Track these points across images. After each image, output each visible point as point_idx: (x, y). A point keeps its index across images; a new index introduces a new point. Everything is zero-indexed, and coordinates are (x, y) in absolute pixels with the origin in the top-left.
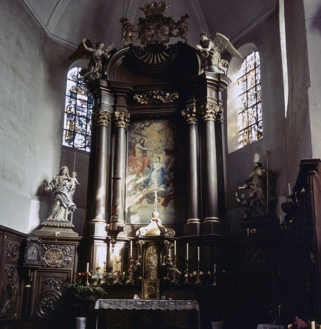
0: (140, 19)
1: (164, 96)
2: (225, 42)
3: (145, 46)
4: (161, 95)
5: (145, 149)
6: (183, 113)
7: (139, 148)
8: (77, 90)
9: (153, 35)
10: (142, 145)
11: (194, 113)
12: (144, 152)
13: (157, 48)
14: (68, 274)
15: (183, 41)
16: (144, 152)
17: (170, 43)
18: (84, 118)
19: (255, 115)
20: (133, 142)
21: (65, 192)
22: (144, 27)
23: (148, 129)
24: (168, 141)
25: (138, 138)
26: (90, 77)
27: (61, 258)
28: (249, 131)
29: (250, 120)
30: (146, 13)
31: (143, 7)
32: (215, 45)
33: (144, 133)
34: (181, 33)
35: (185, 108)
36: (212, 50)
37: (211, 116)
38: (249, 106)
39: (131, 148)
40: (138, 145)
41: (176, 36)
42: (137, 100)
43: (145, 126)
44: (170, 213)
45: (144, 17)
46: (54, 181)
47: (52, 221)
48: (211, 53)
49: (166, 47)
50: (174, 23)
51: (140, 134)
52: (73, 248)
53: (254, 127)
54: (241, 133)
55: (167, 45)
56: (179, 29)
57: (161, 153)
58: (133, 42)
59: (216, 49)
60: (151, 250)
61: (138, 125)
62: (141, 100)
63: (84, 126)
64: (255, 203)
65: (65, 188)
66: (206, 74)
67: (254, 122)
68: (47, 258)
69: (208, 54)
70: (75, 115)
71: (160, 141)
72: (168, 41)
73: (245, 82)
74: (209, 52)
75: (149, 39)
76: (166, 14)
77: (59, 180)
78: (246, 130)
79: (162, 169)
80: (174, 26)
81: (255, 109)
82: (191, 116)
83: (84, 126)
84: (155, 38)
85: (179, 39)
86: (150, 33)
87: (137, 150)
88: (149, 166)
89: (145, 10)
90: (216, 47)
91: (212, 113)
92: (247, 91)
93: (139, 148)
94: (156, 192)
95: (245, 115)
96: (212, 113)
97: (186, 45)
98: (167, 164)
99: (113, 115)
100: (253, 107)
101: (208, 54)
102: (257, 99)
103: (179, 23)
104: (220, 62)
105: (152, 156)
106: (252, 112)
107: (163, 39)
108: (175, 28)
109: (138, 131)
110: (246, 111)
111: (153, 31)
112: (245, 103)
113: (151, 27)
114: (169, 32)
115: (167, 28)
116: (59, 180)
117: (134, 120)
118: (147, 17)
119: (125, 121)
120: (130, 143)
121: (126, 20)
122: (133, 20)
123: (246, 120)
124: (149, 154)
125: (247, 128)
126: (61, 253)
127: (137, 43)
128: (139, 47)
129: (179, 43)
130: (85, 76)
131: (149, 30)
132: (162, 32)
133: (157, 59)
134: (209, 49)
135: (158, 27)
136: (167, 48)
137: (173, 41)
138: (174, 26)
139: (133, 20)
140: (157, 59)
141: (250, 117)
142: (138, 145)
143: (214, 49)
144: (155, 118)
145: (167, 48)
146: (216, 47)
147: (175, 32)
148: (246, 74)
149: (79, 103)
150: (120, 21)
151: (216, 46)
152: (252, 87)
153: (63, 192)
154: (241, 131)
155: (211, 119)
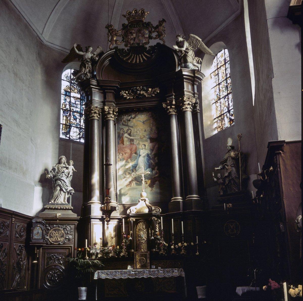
0: (123, 25)
1: (147, 91)
2: (197, 41)
3: (129, 48)
4: (144, 90)
5: (132, 138)
6: (164, 105)
7: (127, 138)
8: (71, 89)
9: (135, 38)
10: (130, 134)
11: (173, 105)
12: (132, 141)
13: (138, 49)
14: (69, 250)
15: (162, 42)
16: (132, 141)
17: (150, 44)
18: (78, 113)
19: (227, 104)
20: (121, 132)
21: (64, 178)
22: (126, 32)
23: (134, 120)
24: (151, 130)
25: (126, 129)
26: (82, 77)
27: (62, 236)
28: (222, 119)
29: (222, 109)
30: (128, 19)
31: (125, 14)
32: (189, 45)
33: (131, 124)
34: (159, 35)
35: (165, 101)
36: (187, 49)
37: (188, 107)
38: (221, 97)
39: (120, 138)
40: (126, 135)
41: (155, 38)
42: (123, 96)
43: (131, 118)
44: (156, 193)
45: (126, 22)
46: (54, 169)
47: (54, 204)
48: (186, 52)
49: (147, 48)
50: (153, 27)
51: (127, 125)
52: (73, 227)
53: (226, 115)
54: (215, 121)
55: (147, 46)
56: (157, 31)
57: (146, 141)
58: (118, 45)
59: (190, 48)
60: (141, 226)
61: (125, 118)
62: (127, 95)
63: (78, 120)
64: (230, 181)
65: (64, 175)
66: (182, 70)
67: (226, 111)
68: (51, 237)
69: (183, 53)
70: (70, 111)
71: (145, 131)
72: (149, 43)
73: (217, 76)
74: (184, 51)
75: (132, 42)
76: (146, 19)
77: (58, 168)
78: (220, 118)
79: (148, 155)
80: (153, 30)
81: (226, 100)
82: (171, 108)
83: (78, 120)
84: (137, 40)
85: (158, 41)
86: (132, 37)
87: (125, 139)
88: (136, 153)
89: (127, 17)
90: (190, 46)
91: (189, 104)
92: (219, 84)
93: (127, 138)
94: (143, 175)
95: (218, 104)
96: (189, 104)
97: (164, 46)
98: (152, 150)
99: (103, 109)
100: (224, 97)
101: (183, 53)
102: (228, 91)
103: (157, 27)
104: (194, 60)
105: (139, 144)
106: (224, 102)
107: (144, 41)
108: (154, 32)
109: (125, 123)
110: (219, 101)
111: (134, 35)
112: (217, 94)
113: (133, 31)
114: (149, 35)
115: (147, 32)
116: (58, 168)
117: (121, 113)
118: (129, 23)
119: (113, 114)
120: (119, 133)
121: (111, 26)
122: (117, 26)
123: (219, 109)
124: (135, 142)
125: (220, 116)
126: (63, 232)
127: (122, 46)
128: (123, 49)
129: (158, 44)
130: (77, 76)
131: (132, 34)
132: (143, 36)
133: (139, 59)
134: (184, 49)
135: (139, 31)
136: (148, 49)
137: (153, 43)
138: (153, 30)
139: (117, 26)
140: (139, 59)
141: (223, 106)
142: (126, 135)
143: (189, 48)
144: (139, 111)
145: (148, 49)
146: (190, 46)
147: (154, 35)
148: (218, 69)
149: (73, 100)
150: (106, 27)
151: (190, 45)
152: (223, 80)
153: (62, 178)
154: (215, 119)
155: (189, 109)
